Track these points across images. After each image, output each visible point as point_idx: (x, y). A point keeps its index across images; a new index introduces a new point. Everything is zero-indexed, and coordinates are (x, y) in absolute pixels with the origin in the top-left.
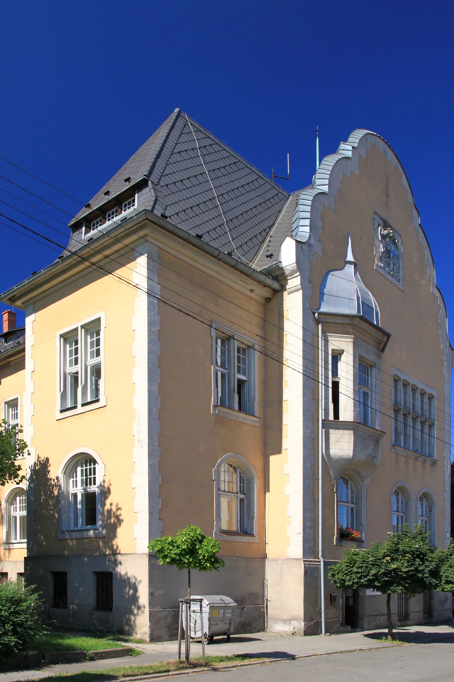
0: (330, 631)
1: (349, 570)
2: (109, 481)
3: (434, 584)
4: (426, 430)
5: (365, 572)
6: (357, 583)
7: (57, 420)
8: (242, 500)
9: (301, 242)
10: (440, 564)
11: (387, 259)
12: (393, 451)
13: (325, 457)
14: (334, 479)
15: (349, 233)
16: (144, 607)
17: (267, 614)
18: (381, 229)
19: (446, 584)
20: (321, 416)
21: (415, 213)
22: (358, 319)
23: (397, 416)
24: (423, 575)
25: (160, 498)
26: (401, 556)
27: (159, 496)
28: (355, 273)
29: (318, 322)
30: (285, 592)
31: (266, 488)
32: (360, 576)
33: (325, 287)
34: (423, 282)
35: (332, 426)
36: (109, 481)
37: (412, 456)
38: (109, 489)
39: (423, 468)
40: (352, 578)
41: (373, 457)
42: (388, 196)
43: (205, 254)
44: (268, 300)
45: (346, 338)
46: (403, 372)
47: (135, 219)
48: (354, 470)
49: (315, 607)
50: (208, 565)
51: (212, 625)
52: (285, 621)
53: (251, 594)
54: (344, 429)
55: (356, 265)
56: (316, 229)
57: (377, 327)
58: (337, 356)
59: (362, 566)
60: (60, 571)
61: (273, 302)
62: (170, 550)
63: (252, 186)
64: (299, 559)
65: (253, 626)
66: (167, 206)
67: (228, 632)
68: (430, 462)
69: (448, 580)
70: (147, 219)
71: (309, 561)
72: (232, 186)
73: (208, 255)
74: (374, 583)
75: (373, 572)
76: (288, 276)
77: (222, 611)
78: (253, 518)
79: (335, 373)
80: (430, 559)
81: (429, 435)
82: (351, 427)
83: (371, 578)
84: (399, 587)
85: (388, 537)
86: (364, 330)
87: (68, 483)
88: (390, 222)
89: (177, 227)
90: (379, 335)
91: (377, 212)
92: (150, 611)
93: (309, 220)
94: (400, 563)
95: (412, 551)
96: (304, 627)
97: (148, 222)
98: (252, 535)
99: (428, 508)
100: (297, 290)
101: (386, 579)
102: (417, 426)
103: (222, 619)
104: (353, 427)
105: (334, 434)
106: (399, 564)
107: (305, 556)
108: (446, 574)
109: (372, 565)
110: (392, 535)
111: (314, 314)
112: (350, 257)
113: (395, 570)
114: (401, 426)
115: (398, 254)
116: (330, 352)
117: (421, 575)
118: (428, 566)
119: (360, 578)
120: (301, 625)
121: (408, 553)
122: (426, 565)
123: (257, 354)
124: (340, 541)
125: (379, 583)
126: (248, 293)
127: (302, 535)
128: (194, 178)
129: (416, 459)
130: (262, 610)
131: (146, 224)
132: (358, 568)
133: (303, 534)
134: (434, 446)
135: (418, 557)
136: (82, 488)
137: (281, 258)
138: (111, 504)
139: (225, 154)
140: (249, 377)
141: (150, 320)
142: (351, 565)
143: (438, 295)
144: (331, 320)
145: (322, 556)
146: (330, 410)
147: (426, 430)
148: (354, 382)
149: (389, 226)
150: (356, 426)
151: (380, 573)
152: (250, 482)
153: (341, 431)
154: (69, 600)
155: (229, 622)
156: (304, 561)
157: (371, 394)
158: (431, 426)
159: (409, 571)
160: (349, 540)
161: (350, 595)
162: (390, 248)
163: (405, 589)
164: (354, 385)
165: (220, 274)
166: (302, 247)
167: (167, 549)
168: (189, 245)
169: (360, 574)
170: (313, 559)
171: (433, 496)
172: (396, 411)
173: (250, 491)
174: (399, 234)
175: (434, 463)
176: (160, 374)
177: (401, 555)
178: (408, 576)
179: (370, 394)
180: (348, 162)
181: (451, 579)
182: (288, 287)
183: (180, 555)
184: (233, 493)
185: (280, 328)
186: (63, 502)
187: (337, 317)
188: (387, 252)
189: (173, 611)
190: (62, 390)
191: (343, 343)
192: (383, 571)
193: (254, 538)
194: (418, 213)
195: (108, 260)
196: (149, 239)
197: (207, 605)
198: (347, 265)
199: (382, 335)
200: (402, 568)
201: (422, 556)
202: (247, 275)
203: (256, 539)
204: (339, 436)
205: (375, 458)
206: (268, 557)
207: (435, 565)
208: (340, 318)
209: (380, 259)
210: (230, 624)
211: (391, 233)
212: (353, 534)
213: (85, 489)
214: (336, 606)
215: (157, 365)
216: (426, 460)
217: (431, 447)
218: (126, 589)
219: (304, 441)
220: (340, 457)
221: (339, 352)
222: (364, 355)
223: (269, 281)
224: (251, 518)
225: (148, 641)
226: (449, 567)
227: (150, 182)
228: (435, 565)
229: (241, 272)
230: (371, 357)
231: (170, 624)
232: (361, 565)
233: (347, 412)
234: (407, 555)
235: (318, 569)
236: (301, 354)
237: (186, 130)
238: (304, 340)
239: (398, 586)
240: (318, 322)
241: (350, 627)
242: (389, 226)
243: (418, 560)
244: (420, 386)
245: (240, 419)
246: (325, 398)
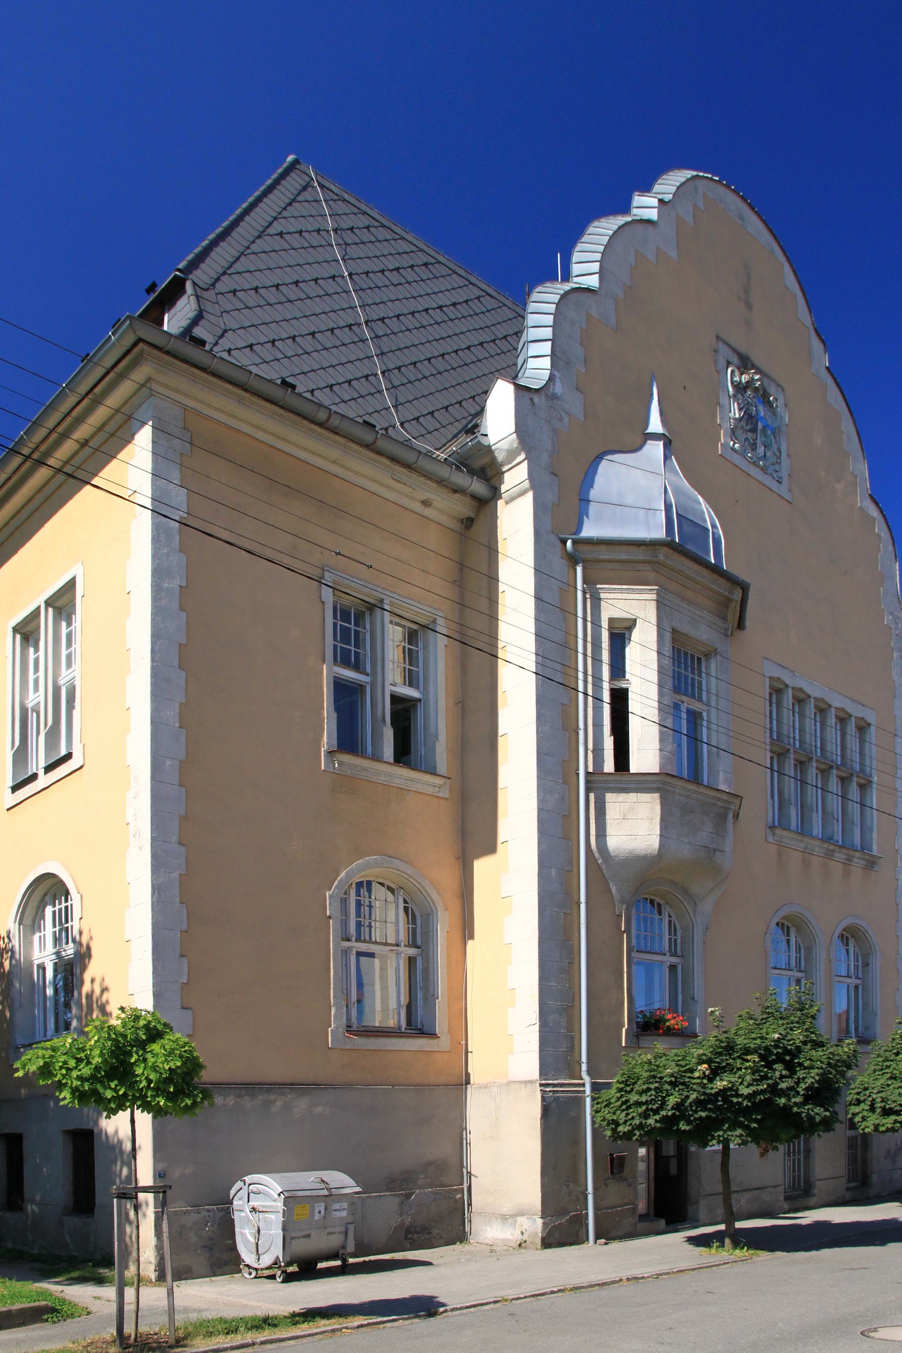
0: (605, 1234)
1: (624, 1099)
2: (90, 930)
3: (818, 1119)
4: (854, 792)
5: (656, 1102)
6: (640, 1126)
7: (8, 810)
8: (411, 960)
9: (528, 389)
10: (831, 1073)
11: (750, 435)
12: (771, 839)
13: (597, 855)
14: (622, 902)
15: (653, 378)
16: (147, 1204)
17: (470, 1204)
18: (733, 372)
19: (883, 1115)
20: (584, 764)
21: (817, 345)
22: (665, 549)
23: (766, 759)
24: (789, 1100)
25: (185, 960)
26: (739, 1061)
27: (182, 956)
28: (666, 458)
29: (573, 560)
30: (504, 1155)
31: (466, 929)
32: (645, 1111)
33: (592, 486)
34: (838, 486)
35: (611, 785)
36: (90, 930)
37: (817, 849)
38: (89, 948)
39: (847, 874)
40: (630, 1117)
41: (711, 851)
42: (749, 306)
43: (299, 419)
44: (468, 523)
45: (641, 592)
46: (793, 672)
47: (114, 344)
48: (673, 883)
49: (571, 1184)
50: (162, 1104)
51: (292, 1238)
52: (504, 1218)
53: (430, 1164)
54: (637, 791)
55: (670, 441)
56: (568, 363)
57: (716, 569)
58: (620, 635)
59: (649, 1089)
60: (12, 1131)
61: (477, 528)
62: (68, 1069)
63: (463, 310)
64: (531, 1082)
65: (435, 1232)
66: (225, 331)
67: (341, 1252)
68: (864, 862)
69: (887, 1107)
70: (140, 340)
71: (554, 1085)
72: (412, 305)
73: (305, 422)
74: (678, 1124)
75: (672, 1100)
76: (502, 465)
77: (320, 1207)
78: (435, 997)
79: (618, 669)
80: (807, 1064)
81: (842, 797)
82: (655, 785)
83: (670, 1113)
84: (735, 1130)
85: (710, 1018)
87: (29, 944)
88: (756, 357)
89: (251, 372)
90: (721, 586)
91: (722, 336)
92: (155, 1213)
93: (550, 343)
94: (737, 1075)
95: (767, 1049)
96: (543, 1230)
97: (146, 348)
98: (433, 1035)
99: (860, 959)
100: (522, 493)
101: (703, 1114)
102: (830, 785)
103: (324, 1224)
104: (660, 785)
105: (616, 803)
106: (734, 1078)
107: (546, 1074)
108: (883, 1095)
109: (670, 1083)
110: (717, 1013)
111: (564, 542)
112: (655, 425)
113: (723, 1092)
114: (790, 787)
115: (775, 426)
116: (605, 624)
117: (783, 1100)
118: (804, 1078)
119: (645, 1115)
120: (535, 1226)
121: (755, 1051)
122: (798, 1078)
123: (442, 641)
124: (637, 1036)
125: (688, 1125)
126: (418, 508)
127: (537, 1027)
128: (426, 362)
129: (829, 855)
130: (459, 1196)
131: (141, 353)
132: (641, 1093)
133: (540, 1027)
134: (871, 829)
135: (780, 1059)
136: (55, 950)
137: (486, 427)
138: (93, 981)
139: (403, 246)
140: (426, 692)
141: (158, 564)
142: (628, 1089)
143: (874, 512)
144: (604, 553)
145: (589, 1072)
146: (606, 752)
147: (854, 792)
148: (661, 685)
149: (753, 366)
150: (664, 783)
151: (688, 1102)
152: (428, 919)
153: (632, 796)
154: (27, 1194)
155: (343, 1229)
156: (541, 1085)
157: (708, 712)
158: (864, 787)
159: (755, 1093)
160: (659, 1035)
161: (672, 1153)
162: (757, 410)
163: (747, 1135)
164: (661, 694)
165: (342, 466)
166: (531, 400)
167: (61, 1068)
168: (255, 399)
169: (644, 1107)
170: (565, 1079)
171: (870, 932)
172: (780, 754)
173: (430, 935)
174: (779, 385)
175: (871, 864)
176: (184, 683)
177: (739, 1057)
178: (754, 1103)
179: (705, 714)
180: (650, 228)
181: (893, 1106)
182: (503, 488)
183: (93, 1078)
184: (386, 944)
185: (493, 579)
186: (17, 985)
187: (617, 548)
188: (749, 419)
189: (219, 1210)
190: (17, 743)
191: (633, 605)
192: (694, 1096)
193: (436, 1041)
194: (824, 344)
195: (87, 451)
196: (154, 386)
197: (279, 1195)
198: (649, 442)
199: (728, 585)
200: (741, 1087)
201: (788, 1058)
202: (407, 466)
203: (444, 1042)
204: (627, 806)
205: (718, 854)
206: (472, 1081)
207: (818, 1074)
208: (624, 548)
209: (733, 433)
210: (346, 1233)
211: (758, 380)
212: (668, 1020)
213: (58, 953)
214: (625, 1179)
215: (176, 663)
216: (853, 856)
217: (865, 830)
218: (116, 1165)
219: (540, 821)
220: (631, 852)
221: (629, 624)
222: (685, 628)
223: (461, 479)
224: (431, 997)
225: (154, 1280)
226: (891, 1078)
227: (189, 286)
228: (818, 1074)
229: (394, 459)
230: (704, 632)
231: (211, 1239)
232: (645, 1087)
233: (645, 755)
234: (749, 1057)
235: (578, 1101)
236: (532, 629)
237: (306, 195)
238: (538, 598)
239: (732, 1128)
240: (575, 559)
241: (662, 1222)
242: (753, 366)
243: (778, 1067)
244: (837, 701)
245: (397, 781)
246: (594, 725)
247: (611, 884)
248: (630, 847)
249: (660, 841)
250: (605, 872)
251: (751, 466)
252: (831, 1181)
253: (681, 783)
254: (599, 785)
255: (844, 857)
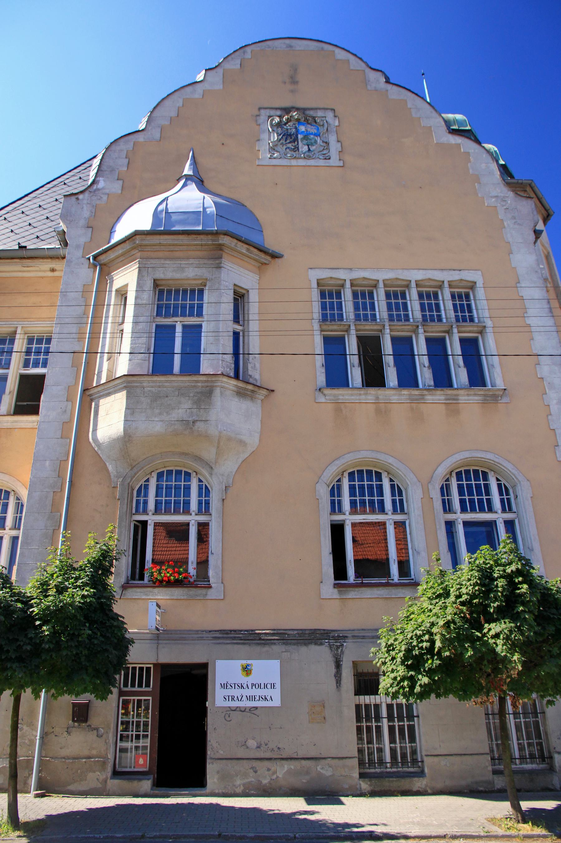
35: (101, 394)
45: (131, 267)
86: (160, 245)
104: (125, 385)
150: (129, 382)
187: (116, 248)
208: (119, 247)
245: (5, 424)
247: (107, 464)
248: (109, 435)
249: (125, 424)
250: (101, 455)
251: (292, 161)
252: (458, 758)
253: (146, 378)
254: (96, 396)
255: (443, 398)
